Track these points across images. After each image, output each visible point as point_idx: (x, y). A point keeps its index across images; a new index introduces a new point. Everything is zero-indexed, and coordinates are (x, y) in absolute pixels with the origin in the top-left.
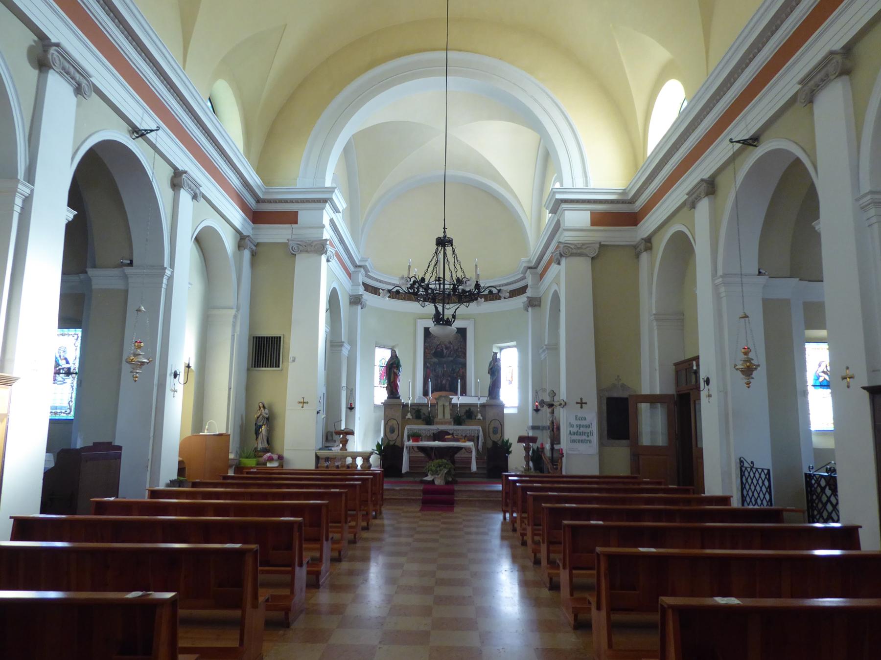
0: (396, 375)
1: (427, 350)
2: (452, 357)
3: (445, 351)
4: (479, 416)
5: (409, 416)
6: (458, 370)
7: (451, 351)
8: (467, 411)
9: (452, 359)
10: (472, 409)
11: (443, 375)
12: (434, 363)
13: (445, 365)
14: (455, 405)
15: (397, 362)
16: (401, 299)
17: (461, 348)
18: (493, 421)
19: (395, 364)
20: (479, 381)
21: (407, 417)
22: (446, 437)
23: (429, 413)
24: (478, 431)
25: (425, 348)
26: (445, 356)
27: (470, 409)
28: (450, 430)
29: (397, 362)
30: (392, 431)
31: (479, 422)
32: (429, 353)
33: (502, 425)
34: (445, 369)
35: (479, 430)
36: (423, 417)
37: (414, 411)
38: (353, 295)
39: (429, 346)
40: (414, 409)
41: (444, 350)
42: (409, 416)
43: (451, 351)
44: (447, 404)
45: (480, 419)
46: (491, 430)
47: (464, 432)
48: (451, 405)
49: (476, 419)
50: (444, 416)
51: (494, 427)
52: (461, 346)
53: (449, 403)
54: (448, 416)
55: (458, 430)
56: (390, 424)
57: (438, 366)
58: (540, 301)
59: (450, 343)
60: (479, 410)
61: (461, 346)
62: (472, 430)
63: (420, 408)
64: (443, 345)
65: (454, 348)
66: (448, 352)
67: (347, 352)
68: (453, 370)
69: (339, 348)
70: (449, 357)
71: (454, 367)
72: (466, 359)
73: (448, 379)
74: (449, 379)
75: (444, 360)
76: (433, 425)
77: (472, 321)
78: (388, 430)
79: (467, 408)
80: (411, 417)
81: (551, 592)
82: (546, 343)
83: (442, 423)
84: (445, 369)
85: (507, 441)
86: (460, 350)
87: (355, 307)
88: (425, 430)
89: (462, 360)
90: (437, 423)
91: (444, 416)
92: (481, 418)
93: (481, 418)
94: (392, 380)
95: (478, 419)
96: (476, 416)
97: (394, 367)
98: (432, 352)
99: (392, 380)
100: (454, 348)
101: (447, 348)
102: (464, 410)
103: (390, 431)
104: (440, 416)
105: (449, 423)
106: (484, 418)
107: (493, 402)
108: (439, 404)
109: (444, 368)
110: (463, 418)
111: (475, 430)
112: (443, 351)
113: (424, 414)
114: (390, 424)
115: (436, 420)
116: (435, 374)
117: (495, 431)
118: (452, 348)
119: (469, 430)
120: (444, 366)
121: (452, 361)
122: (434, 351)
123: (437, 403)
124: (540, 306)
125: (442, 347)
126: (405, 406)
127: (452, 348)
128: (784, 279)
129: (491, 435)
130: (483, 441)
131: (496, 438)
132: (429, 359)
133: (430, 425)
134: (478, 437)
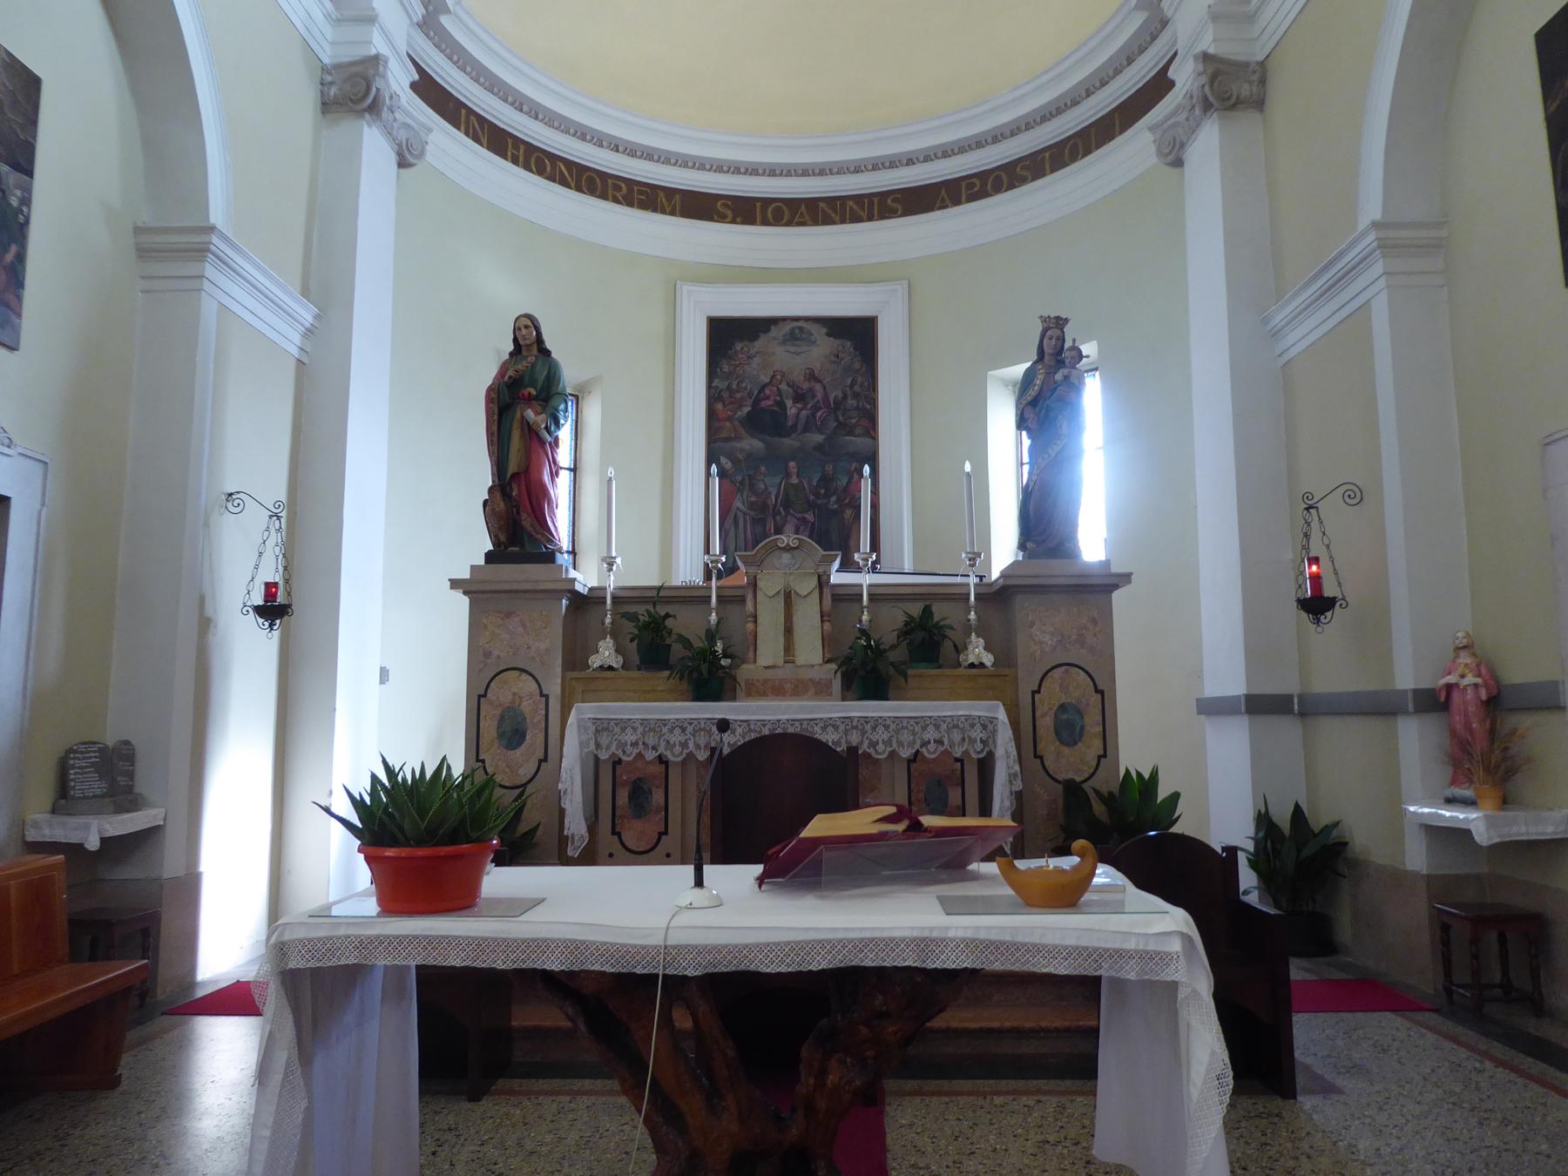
0: (538, 443)
1: (719, 406)
2: (820, 430)
3: (792, 410)
4: (977, 651)
5: (606, 653)
6: (845, 481)
7: (816, 408)
8: (910, 620)
9: (818, 438)
10: (940, 611)
11: (787, 504)
12: (750, 456)
13: (792, 464)
14: (849, 596)
15: (541, 376)
16: (616, 200)
17: (856, 396)
18: (1057, 673)
19: (533, 384)
20: (968, 467)
21: (595, 661)
22: (820, 826)
23: (711, 636)
24: (988, 725)
25: (713, 397)
26: (794, 427)
27: (927, 612)
28: (827, 724)
29: (541, 376)
30: (513, 735)
31: (982, 683)
32: (729, 419)
33: (1104, 695)
34: (794, 480)
35: (993, 720)
36: (677, 651)
37: (629, 628)
38: (338, 67)
39: (729, 388)
40: (633, 617)
41: (789, 403)
42: (606, 653)
43: (816, 408)
44: (807, 586)
45: (982, 665)
46: (1046, 723)
47: (906, 737)
48: (827, 592)
49: (959, 665)
50: (789, 648)
51: (1063, 708)
52: (857, 388)
53: (814, 582)
54: (810, 650)
55: (877, 723)
56: (501, 694)
57: (763, 469)
58: (1263, 81)
59: (812, 376)
60: (972, 615)
61: (857, 388)
62: (954, 724)
63: (662, 610)
64: (783, 387)
65: (826, 396)
66: (804, 413)
67: (297, 338)
68: (826, 480)
69: (190, 269)
70: (805, 430)
71: (829, 468)
72: (875, 438)
73: (804, 520)
74: (810, 517)
75: (789, 442)
76: (734, 699)
77: (901, 289)
78: (489, 729)
79: (915, 610)
80: (617, 662)
81: (373, 52)
82: (1372, 208)
83: (776, 690)
84: (794, 480)
85: (1149, 785)
86: (851, 402)
87: (347, 126)
88: (682, 726)
89: (858, 442)
90: (758, 690)
91: (789, 648)
92: (988, 659)
93: (988, 659)
94: (512, 467)
95: (972, 665)
96: (959, 649)
97: (529, 400)
98: (739, 413)
99: (512, 467)
100: (826, 396)
101: (799, 397)
102: (894, 618)
103: (501, 735)
104: (769, 651)
105: (822, 690)
106: (1006, 658)
107: (1052, 569)
108: (760, 584)
109: (788, 476)
110: (893, 656)
111: (971, 721)
112: (782, 405)
113: (687, 643)
114: (501, 694)
115: (745, 672)
116: (753, 499)
117: (1069, 729)
118: (819, 396)
119: (937, 723)
120: (787, 468)
121: (819, 448)
122: (746, 410)
123: (754, 584)
124: (1259, 104)
125: (780, 392)
126: (584, 603)
127: (819, 396)
128: (611, 775)
129: (1049, 747)
130: (1018, 785)
131: (1069, 763)
132: (727, 439)
133: (716, 697)
134: (986, 767)
